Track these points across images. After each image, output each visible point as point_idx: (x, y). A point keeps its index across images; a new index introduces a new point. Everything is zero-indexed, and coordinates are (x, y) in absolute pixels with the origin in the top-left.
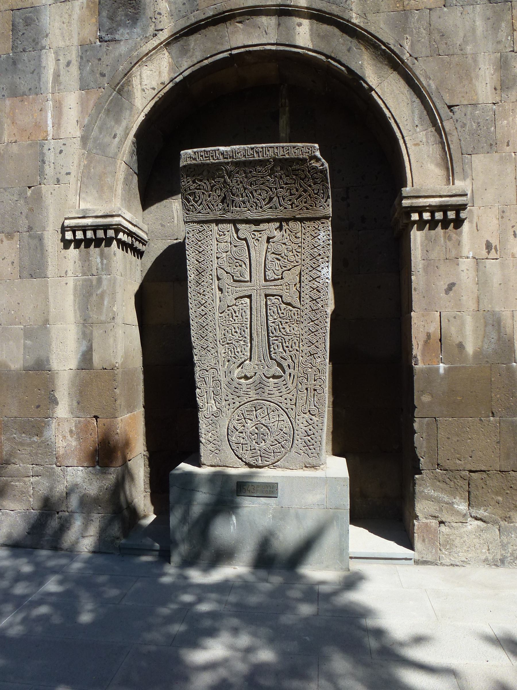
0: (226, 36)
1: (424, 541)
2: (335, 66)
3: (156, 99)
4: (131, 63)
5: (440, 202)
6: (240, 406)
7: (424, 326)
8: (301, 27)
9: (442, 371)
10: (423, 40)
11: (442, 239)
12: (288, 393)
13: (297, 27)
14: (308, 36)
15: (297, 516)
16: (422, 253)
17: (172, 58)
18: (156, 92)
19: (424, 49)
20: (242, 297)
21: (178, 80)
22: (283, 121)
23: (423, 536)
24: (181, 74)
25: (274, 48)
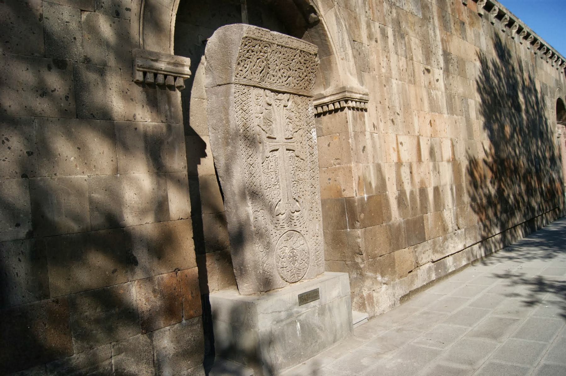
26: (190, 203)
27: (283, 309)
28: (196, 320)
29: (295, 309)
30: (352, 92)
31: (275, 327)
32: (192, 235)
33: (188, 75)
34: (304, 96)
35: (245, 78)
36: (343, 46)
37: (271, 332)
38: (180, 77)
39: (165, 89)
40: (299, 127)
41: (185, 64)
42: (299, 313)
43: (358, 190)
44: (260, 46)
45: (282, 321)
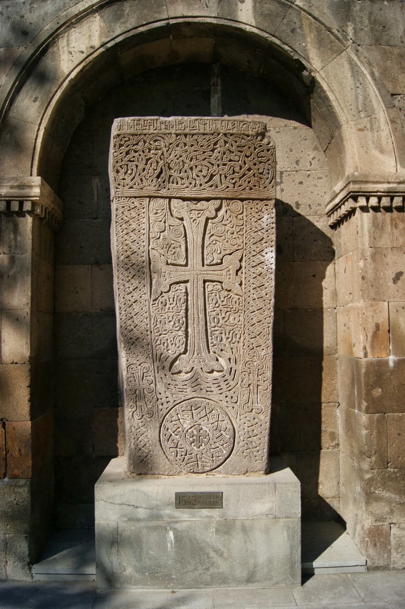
0: (163, 5)
1: (375, 545)
2: (277, 45)
3: (84, 64)
4: (58, 23)
5: (389, 188)
6: (175, 406)
7: (373, 317)
8: (243, 4)
9: (391, 364)
10: (366, 29)
11: (389, 226)
12: (229, 390)
13: (240, 4)
14: (250, 13)
15: (244, 529)
16: (370, 240)
17: (105, 21)
18: (84, 55)
19: (366, 38)
20: (177, 283)
21: (109, 45)
22: (215, 100)
23: (375, 540)
24: (113, 39)
25: (214, 21)
26: (29, 346)
27: (144, 505)
28: (22, 482)
29: (167, 511)
30: (367, 182)
31: (124, 525)
32: (27, 383)
33: (37, 197)
34: (253, 199)
35: (132, 188)
36: (367, 109)
37: (117, 529)
38: (27, 200)
39: (13, 216)
40: (235, 247)
41: (33, 184)
42: (174, 518)
43: (372, 347)
44: (145, 142)
45: (139, 520)
